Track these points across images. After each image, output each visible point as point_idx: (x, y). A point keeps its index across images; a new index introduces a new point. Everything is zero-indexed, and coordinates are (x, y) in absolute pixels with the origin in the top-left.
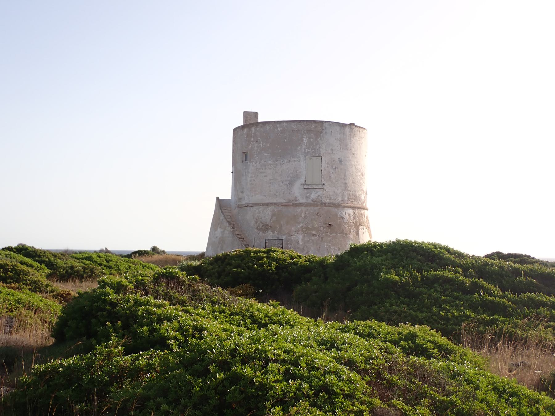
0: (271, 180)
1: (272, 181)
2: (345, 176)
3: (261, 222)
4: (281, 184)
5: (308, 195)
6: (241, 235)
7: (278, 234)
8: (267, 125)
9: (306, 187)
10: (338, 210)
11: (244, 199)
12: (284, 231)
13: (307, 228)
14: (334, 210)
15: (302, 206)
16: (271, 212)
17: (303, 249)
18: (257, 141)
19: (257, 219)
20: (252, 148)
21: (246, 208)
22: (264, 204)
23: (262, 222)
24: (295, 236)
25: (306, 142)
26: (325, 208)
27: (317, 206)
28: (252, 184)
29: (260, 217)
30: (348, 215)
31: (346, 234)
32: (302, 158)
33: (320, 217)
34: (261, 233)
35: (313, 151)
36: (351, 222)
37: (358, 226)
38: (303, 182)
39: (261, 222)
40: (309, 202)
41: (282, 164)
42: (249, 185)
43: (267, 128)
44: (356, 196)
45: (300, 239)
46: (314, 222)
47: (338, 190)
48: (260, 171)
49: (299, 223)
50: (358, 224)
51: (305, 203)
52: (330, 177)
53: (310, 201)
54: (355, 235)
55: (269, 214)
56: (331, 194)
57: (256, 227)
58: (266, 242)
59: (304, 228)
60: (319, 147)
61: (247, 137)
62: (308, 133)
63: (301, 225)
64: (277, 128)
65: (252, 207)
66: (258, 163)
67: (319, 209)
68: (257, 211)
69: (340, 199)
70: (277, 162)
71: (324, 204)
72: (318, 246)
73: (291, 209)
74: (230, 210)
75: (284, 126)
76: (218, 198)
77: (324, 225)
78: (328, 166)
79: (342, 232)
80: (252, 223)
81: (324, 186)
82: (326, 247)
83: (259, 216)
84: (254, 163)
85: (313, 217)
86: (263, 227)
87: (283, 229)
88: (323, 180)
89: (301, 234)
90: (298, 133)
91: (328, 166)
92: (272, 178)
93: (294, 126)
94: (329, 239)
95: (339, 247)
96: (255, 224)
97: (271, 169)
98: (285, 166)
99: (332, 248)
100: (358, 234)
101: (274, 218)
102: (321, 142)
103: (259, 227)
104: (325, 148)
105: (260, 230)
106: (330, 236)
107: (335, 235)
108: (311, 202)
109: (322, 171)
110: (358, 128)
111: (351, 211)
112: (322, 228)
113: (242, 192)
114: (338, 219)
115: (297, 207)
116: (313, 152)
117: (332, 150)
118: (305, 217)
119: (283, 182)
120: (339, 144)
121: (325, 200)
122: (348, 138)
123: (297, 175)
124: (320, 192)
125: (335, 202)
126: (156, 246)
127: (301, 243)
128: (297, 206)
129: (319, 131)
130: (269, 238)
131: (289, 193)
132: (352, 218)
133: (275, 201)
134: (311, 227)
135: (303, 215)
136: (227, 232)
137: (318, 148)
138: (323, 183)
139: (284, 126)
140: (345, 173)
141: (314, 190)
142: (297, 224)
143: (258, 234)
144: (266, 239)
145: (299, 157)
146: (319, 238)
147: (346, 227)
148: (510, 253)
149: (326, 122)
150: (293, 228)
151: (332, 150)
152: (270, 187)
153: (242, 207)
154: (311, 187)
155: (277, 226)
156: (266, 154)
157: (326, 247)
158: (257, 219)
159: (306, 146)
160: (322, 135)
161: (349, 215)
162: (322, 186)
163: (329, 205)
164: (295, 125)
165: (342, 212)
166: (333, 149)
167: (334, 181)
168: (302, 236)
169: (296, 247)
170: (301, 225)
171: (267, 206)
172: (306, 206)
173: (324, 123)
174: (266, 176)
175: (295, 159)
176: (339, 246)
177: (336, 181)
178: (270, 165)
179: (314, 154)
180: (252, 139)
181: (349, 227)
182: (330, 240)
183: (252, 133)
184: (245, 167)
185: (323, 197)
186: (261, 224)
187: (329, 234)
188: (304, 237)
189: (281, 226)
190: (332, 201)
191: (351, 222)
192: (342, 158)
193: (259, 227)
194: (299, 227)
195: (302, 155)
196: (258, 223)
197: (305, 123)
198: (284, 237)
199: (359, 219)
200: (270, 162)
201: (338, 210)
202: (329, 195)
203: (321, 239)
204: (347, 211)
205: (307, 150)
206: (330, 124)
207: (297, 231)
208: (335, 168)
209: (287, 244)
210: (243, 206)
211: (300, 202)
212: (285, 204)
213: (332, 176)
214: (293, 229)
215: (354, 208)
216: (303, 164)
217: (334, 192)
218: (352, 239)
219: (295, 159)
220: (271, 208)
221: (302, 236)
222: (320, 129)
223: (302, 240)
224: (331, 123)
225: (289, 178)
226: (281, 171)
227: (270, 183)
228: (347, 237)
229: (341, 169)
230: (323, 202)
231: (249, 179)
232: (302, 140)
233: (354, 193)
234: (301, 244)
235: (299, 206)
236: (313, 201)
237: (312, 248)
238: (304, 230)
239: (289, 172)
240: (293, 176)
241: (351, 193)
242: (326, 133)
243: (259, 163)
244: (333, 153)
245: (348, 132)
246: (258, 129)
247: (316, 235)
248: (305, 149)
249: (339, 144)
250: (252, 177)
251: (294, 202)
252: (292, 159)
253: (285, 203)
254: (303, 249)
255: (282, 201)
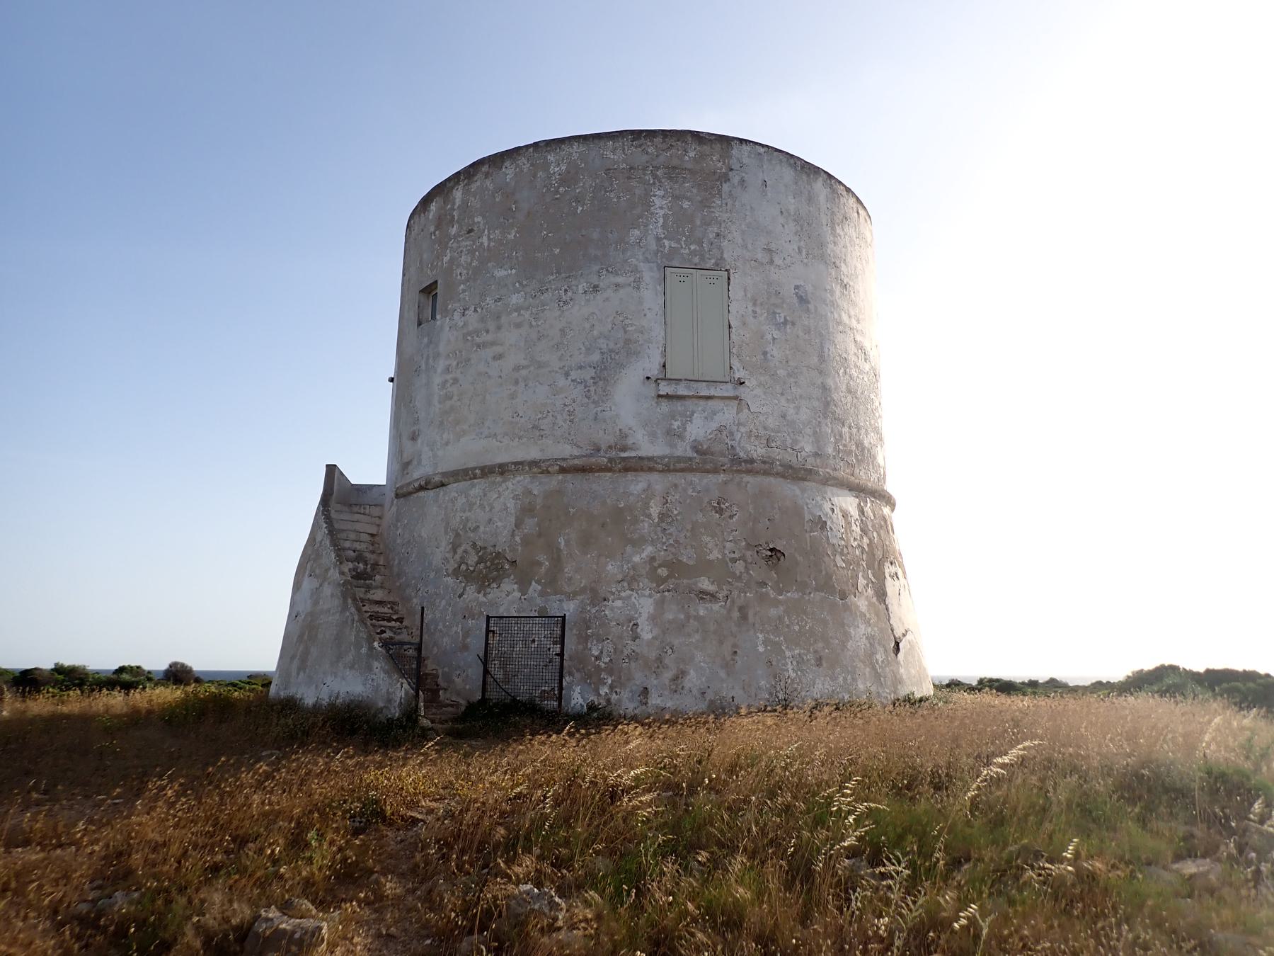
0: (517, 368)
1: (524, 372)
2: (822, 358)
3: (474, 545)
4: (562, 382)
5: (676, 424)
6: (394, 603)
7: (543, 594)
8: (507, 164)
9: (665, 389)
10: (803, 491)
11: (419, 463)
12: (570, 579)
13: (675, 567)
14: (788, 490)
15: (651, 470)
16: (516, 497)
17: (659, 660)
18: (470, 231)
19: (458, 535)
20: (451, 261)
21: (422, 494)
22: (487, 471)
23: (479, 544)
24: (619, 603)
25: (661, 212)
26: (748, 478)
27: (715, 471)
28: (449, 397)
29: (469, 525)
30: (840, 517)
31: (843, 596)
32: (649, 275)
33: (731, 517)
34: (471, 592)
35: (693, 247)
36: (855, 544)
37: (881, 564)
38: (656, 372)
39: (474, 545)
40: (679, 452)
41: (565, 303)
42: (435, 401)
43: (509, 171)
44: (859, 444)
45: (645, 616)
46: (706, 539)
47: (798, 408)
48: (478, 340)
49: (638, 543)
50: (879, 554)
51: (662, 458)
52: (765, 353)
53: (683, 449)
54: (874, 599)
55: (506, 509)
56: (772, 422)
57: (452, 565)
58: (488, 631)
59: (660, 566)
60: (718, 235)
61: (437, 228)
62: (670, 178)
63: (649, 550)
64: (546, 166)
65: (443, 485)
66: (470, 312)
67: (725, 483)
68: (462, 500)
69: (809, 448)
70: (547, 296)
71: (746, 461)
72: (727, 649)
73: (602, 484)
74: (380, 518)
75: (575, 156)
76: (332, 470)
77: (749, 553)
78: (754, 312)
79: (826, 586)
80: (440, 553)
81: (741, 388)
82: (761, 649)
83: (467, 520)
84: (457, 316)
85: (700, 517)
86: (481, 566)
87: (568, 569)
88: (736, 364)
89: (647, 592)
90: (629, 178)
91: (754, 312)
92: (524, 363)
93: (614, 151)
94: (773, 612)
95: (816, 652)
96: (449, 556)
97: (518, 326)
98: (577, 307)
99: (788, 654)
100: (881, 594)
101: (530, 525)
102: (725, 216)
103: (463, 567)
104: (740, 241)
105: (469, 577)
106: (776, 603)
107: (796, 596)
108: (690, 453)
109: (733, 330)
110: (854, 200)
111: (849, 503)
112: (739, 567)
113: (414, 438)
114: (807, 527)
115: (630, 476)
116: (693, 253)
117: (769, 250)
118: (663, 516)
119: (567, 375)
120: (796, 233)
121: (749, 447)
122: (824, 219)
123: (627, 341)
124: (727, 414)
125: (789, 457)
126: (180, 660)
127: (646, 633)
128: (626, 470)
129: (715, 173)
130: (502, 611)
131: (596, 419)
132: (856, 529)
133: (533, 454)
134: (691, 563)
135: (655, 510)
136: (327, 590)
137: (712, 236)
138: (737, 376)
139: (575, 156)
140: (822, 347)
141: (702, 403)
142: (629, 548)
143: (460, 596)
144: (488, 618)
145: (636, 270)
146: (729, 611)
147: (841, 563)
148: (1211, 667)
149: (742, 141)
150: (610, 567)
151: (769, 250)
152: (513, 396)
153: (410, 493)
154: (688, 388)
155: (542, 558)
156: (500, 273)
157: (761, 649)
158: (458, 535)
159: (664, 226)
160: (726, 187)
161: (845, 515)
162: (735, 389)
163: (764, 468)
164: (619, 151)
165: (819, 499)
166: (773, 246)
167: (781, 372)
168: (651, 601)
169: (626, 652)
170: (649, 550)
171: (502, 474)
172: (667, 470)
173: (735, 144)
174: (498, 357)
175: (620, 280)
176: (820, 645)
177: (789, 375)
178: (518, 309)
179: (696, 260)
180: (453, 231)
181: (848, 563)
182: (780, 619)
183: (452, 209)
184: (426, 340)
185: (738, 436)
186: (473, 552)
187: (772, 594)
188: (660, 604)
189: (557, 562)
190: (777, 454)
191: (855, 544)
192: (809, 288)
193: (463, 567)
194: (636, 559)
195: (647, 260)
196: (460, 551)
197: (658, 140)
198: (569, 608)
199: (879, 535)
200: (516, 299)
201: (803, 491)
202: (765, 428)
203: (736, 614)
204: (835, 500)
205: (666, 242)
206: (760, 154)
207: (630, 580)
208: (785, 322)
209: (584, 639)
210: (411, 488)
211: (642, 453)
212: (576, 462)
213: (775, 351)
214: (611, 568)
215: (859, 490)
216: (650, 297)
217: (784, 416)
218: (863, 615)
219: (620, 280)
220: (515, 484)
221: (651, 601)
222: (721, 167)
223: (653, 619)
224: (762, 150)
225: (596, 357)
226: (562, 330)
227: (517, 382)
228: (847, 608)
229: (807, 331)
230: (742, 454)
231: (437, 380)
232: (648, 205)
233: (854, 431)
234: (650, 636)
235: (636, 470)
236: (696, 447)
237: (699, 656)
238: (663, 572)
239: (595, 332)
240: (612, 345)
241: (845, 430)
242: (742, 181)
243: (475, 310)
244: (772, 262)
245: (822, 198)
246: (474, 187)
247: (713, 597)
248: (658, 239)
249: (796, 233)
250: (447, 370)
251: (613, 454)
252: (606, 280)
253: (577, 457)
254: (659, 660)
255: (565, 450)
